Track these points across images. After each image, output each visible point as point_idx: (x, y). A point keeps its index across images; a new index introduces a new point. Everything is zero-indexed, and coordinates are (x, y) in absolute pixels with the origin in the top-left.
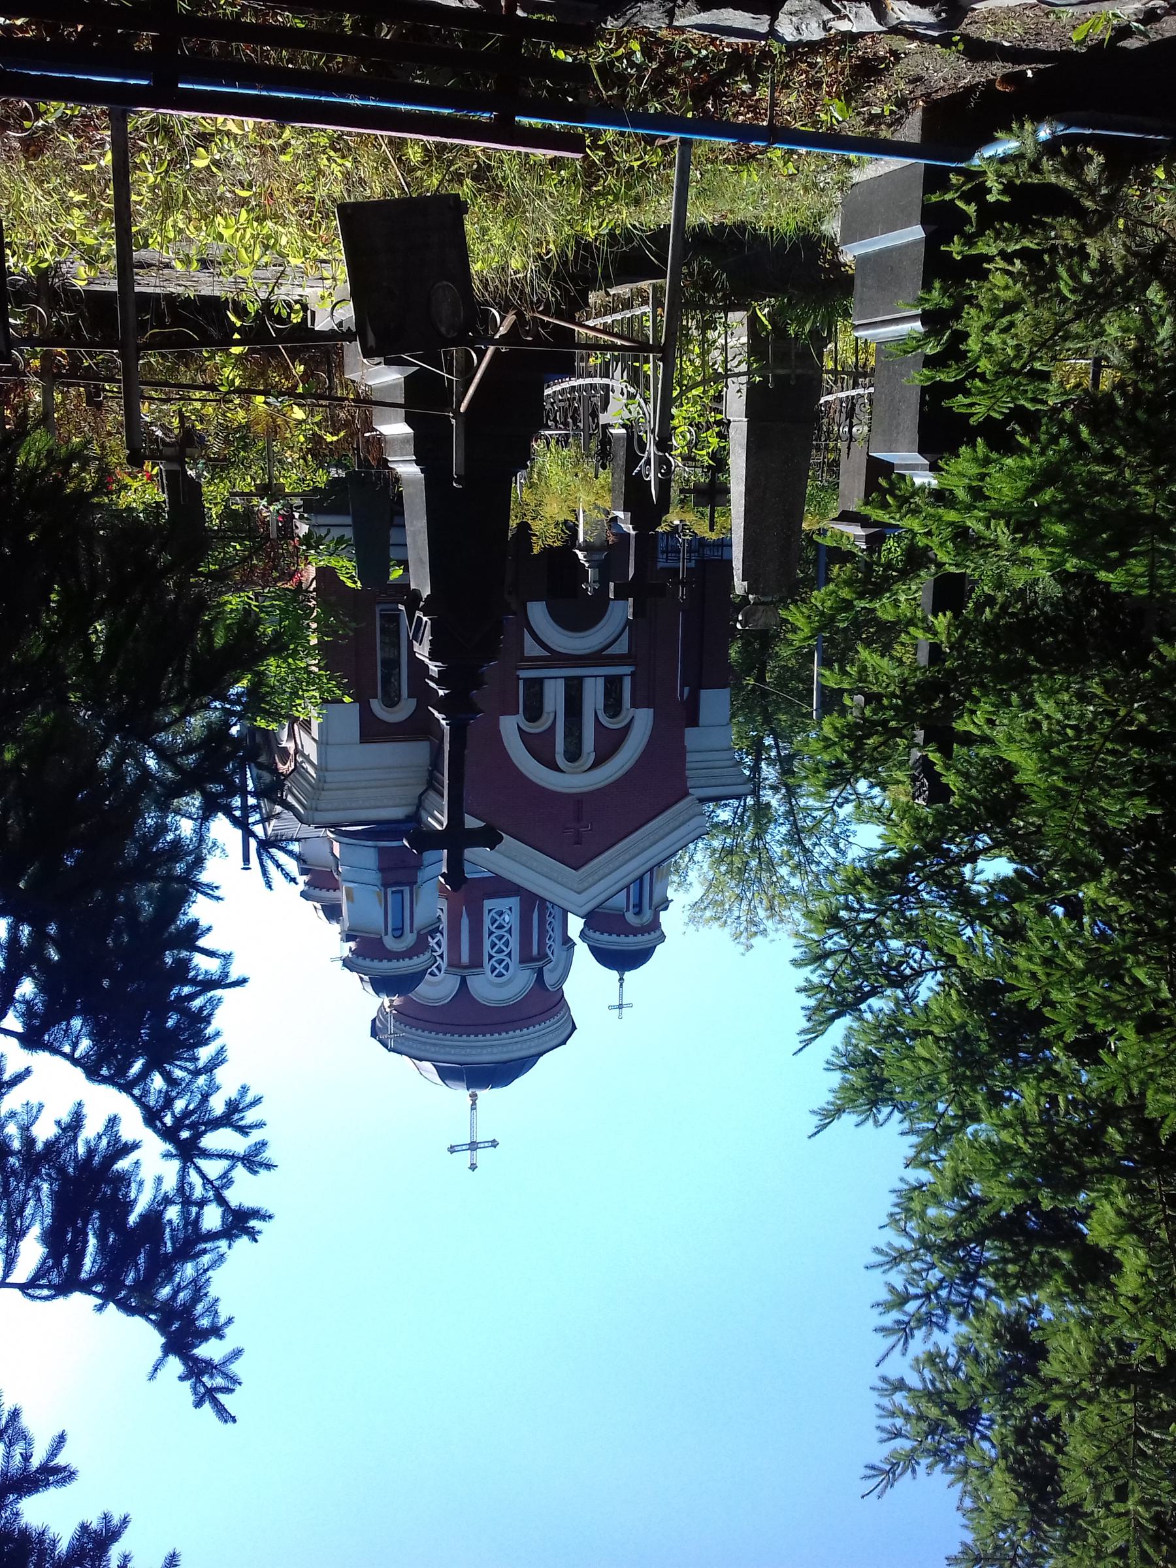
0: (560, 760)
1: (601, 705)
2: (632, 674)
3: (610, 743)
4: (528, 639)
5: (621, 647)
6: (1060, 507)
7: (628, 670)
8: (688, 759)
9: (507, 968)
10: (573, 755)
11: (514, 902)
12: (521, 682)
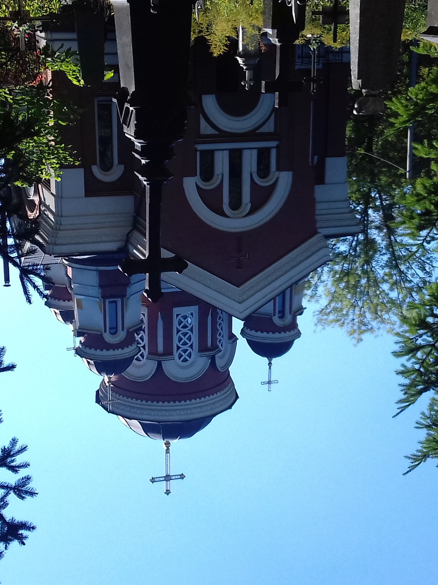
2: (277, 147)
3: (261, 197)
4: (203, 122)
5: (269, 127)
7: (273, 144)
10: (236, 204)
11: (194, 309)
12: (198, 153)
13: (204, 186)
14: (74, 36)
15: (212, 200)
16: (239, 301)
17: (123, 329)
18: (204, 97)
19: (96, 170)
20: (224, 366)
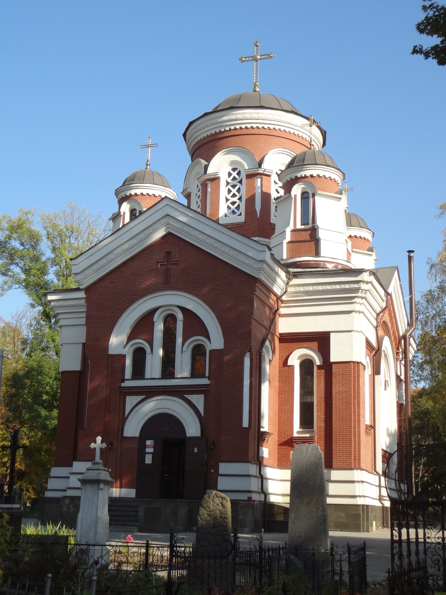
0: (180, 316)
1: (149, 357)
2: (123, 380)
3: (143, 326)
4: (201, 409)
5: (131, 401)
6: (427, 29)
7: (126, 384)
8: (85, 319)
9: (230, 175)
10: (170, 320)
12: (207, 375)
13: (202, 339)
14: (329, 501)
15: (194, 325)
16: (168, 217)
17: (295, 196)
18: (199, 434)
19: (318, 362)
20: (196, 165)
